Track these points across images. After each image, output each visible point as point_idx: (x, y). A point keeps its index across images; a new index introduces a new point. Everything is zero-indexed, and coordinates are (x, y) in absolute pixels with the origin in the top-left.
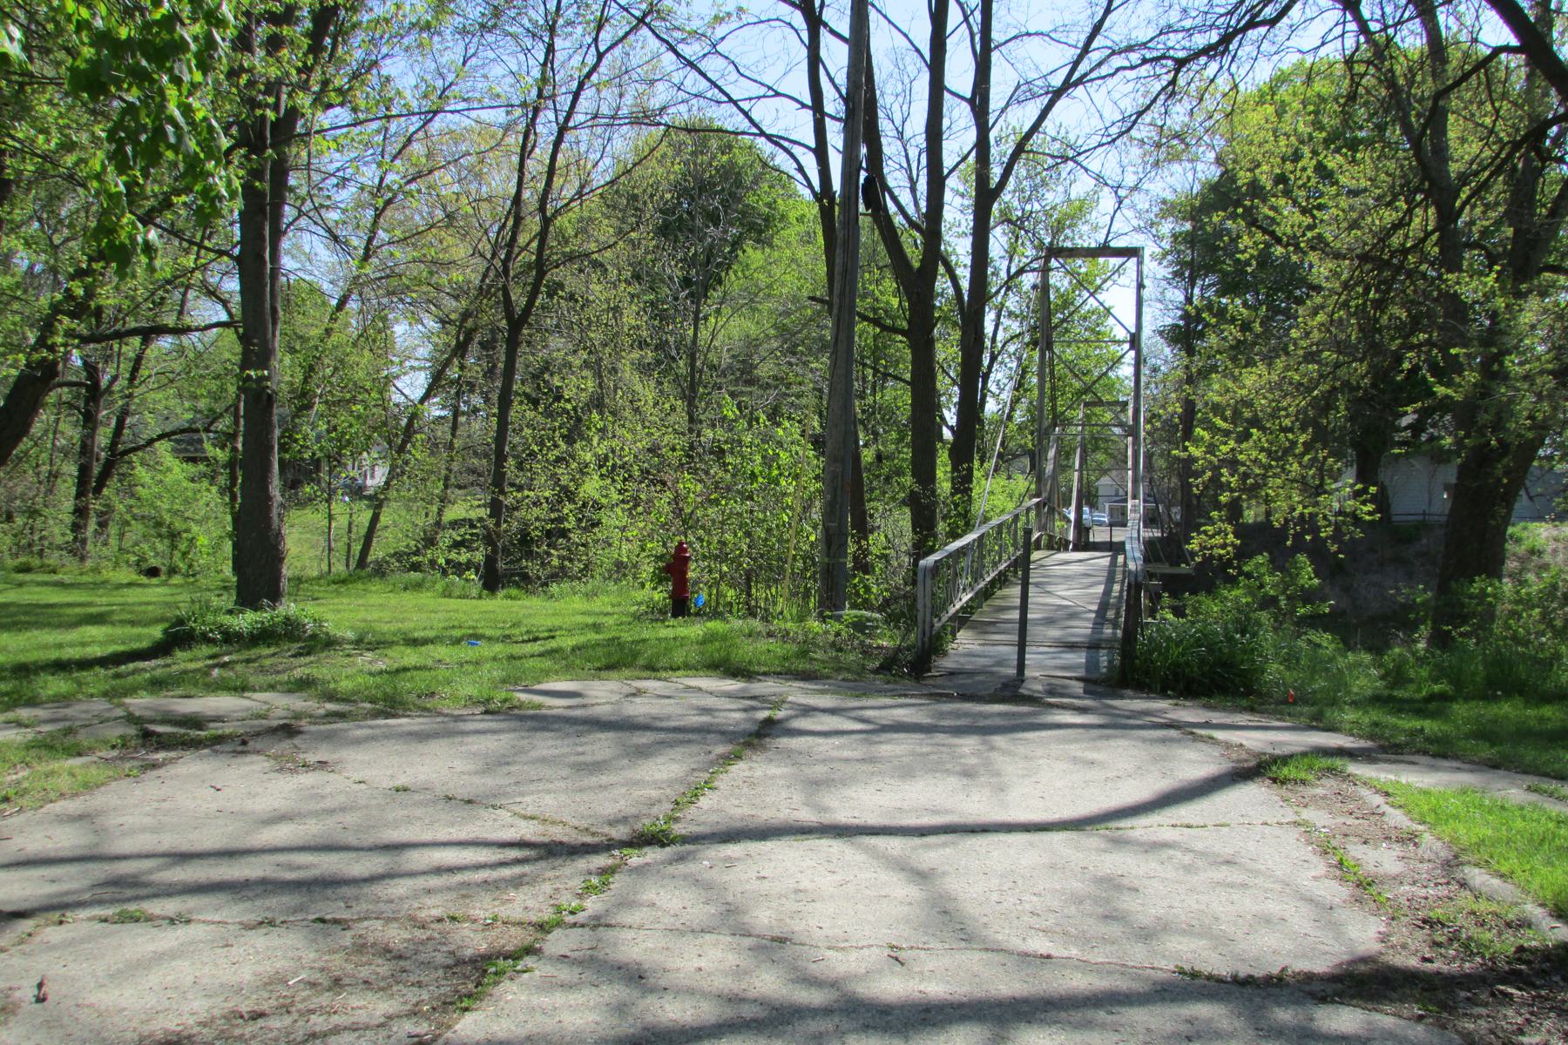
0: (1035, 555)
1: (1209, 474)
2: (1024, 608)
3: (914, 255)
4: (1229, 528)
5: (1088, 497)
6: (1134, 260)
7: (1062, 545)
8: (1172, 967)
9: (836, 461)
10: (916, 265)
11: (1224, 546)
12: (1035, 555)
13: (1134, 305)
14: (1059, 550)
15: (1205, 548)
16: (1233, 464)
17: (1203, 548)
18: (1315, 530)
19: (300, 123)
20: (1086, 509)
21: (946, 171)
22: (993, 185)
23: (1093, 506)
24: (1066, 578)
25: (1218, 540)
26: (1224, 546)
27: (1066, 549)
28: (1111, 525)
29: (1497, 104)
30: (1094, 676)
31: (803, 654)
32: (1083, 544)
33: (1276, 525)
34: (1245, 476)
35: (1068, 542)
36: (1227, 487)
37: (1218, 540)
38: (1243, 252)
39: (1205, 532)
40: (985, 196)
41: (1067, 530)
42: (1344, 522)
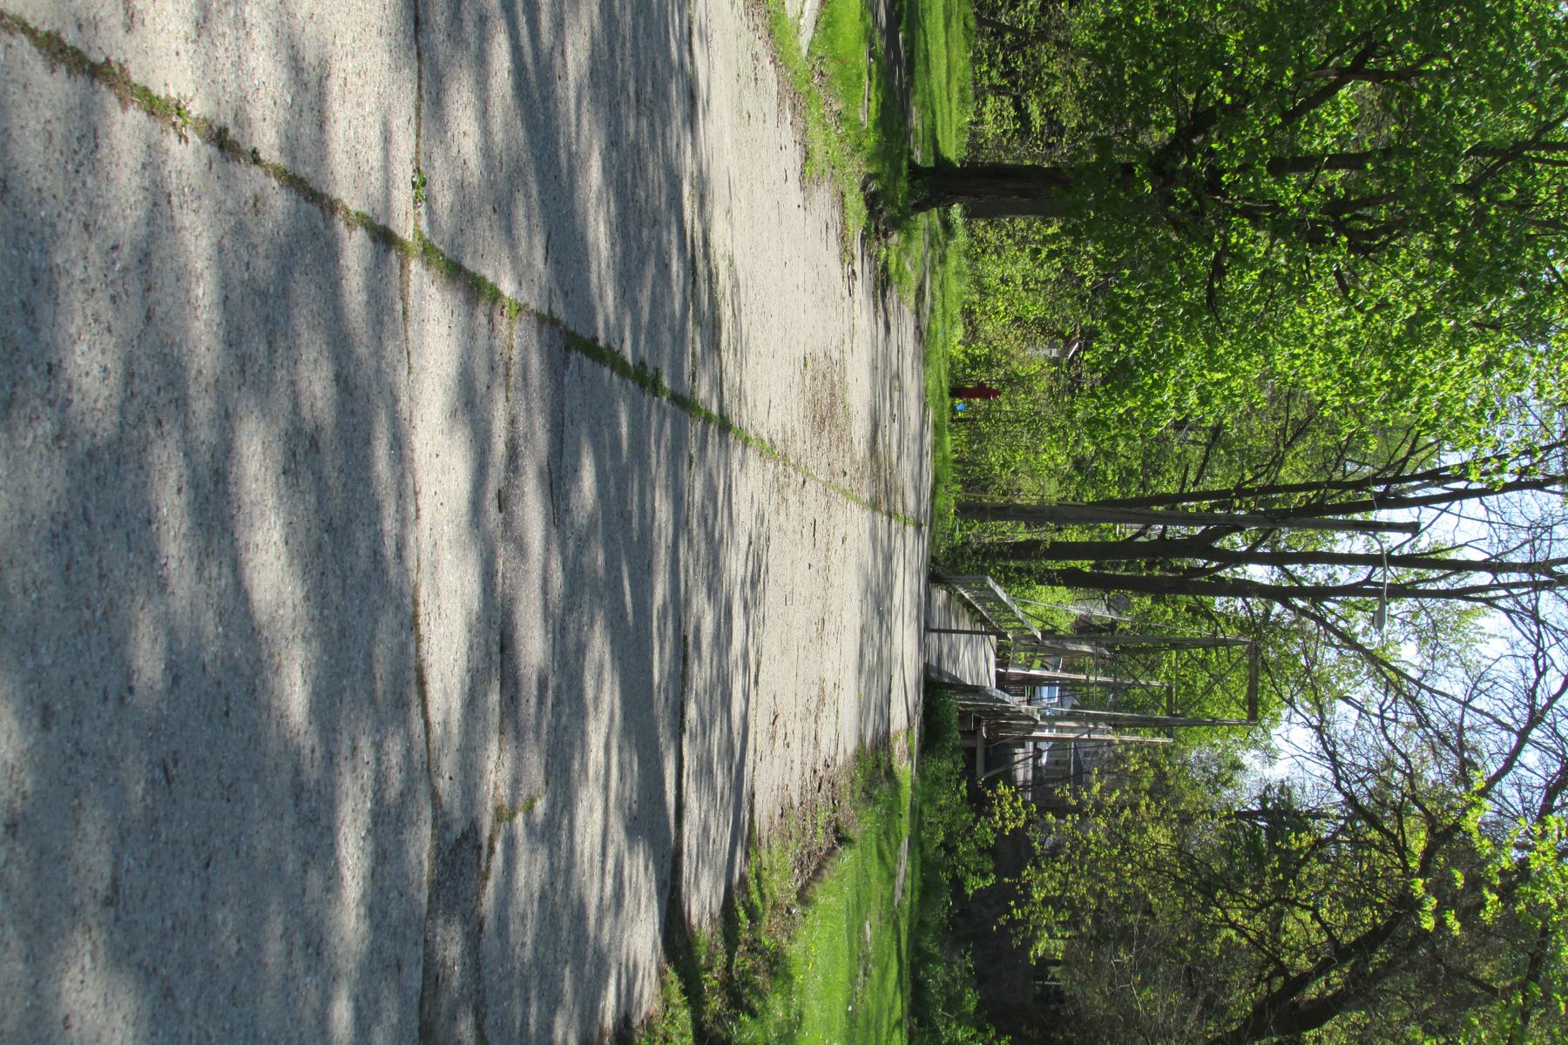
0: (993, 638)
2: (957, 632)
4: (1021, 824)
7: (1002, 662)
8: (864, 318)
10: (1217, 545)
11: (1003, 818)
12: (993, 638)
14: (997, 656)
15: (1000, 800)
17: (1000, 798)
19: (1200, 138)
24: (976, 660)
25: (1009, 813)
26: (1003, 818)
27: (998, 665)
29: (1304, 963)
31: (940, 516)
37: (1009, 813)
39: (1016, 799)
42: (1027, 929)
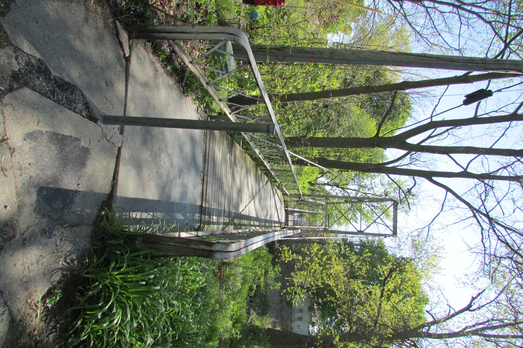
1: (308, 253)
3: (413, 140)
4: (291, 259)
5: (301, 214)
6: (392, 233)
9: (331, 53)
11: (285, 257)
13: (352, 227)
16: (312, 261)
18: (290, 286)
20: (298, 214)
21: (450, 155)
22: (434, 178)
23: (299, 216)
27: (285, 207)
28: (294, 221)
30: (115, 205)
32: (287, 213)
33: (292, 274)
34: (308, 265)
35: (287, 207)
36: (304, 259)
37: (287, 255)
38: (381, 267)
40: (429, 175)
41: (291, 208)
